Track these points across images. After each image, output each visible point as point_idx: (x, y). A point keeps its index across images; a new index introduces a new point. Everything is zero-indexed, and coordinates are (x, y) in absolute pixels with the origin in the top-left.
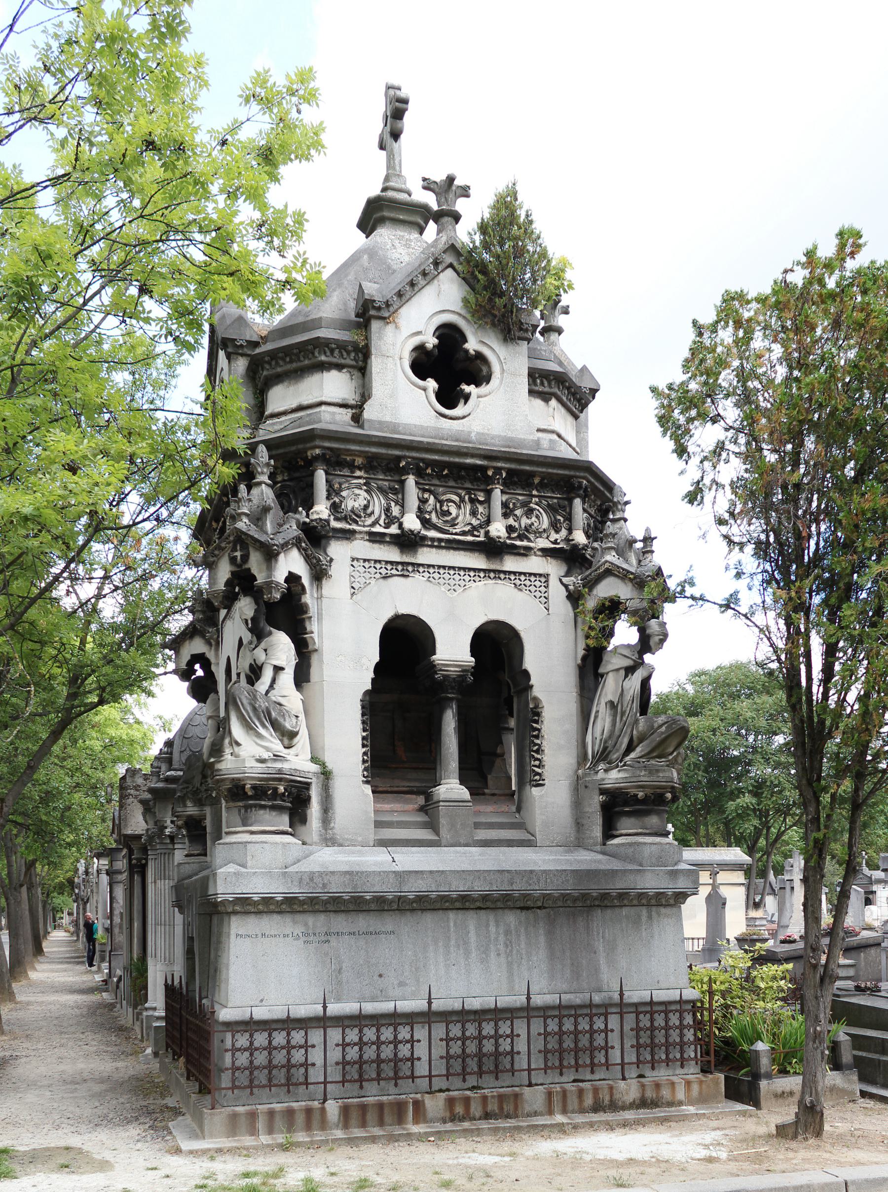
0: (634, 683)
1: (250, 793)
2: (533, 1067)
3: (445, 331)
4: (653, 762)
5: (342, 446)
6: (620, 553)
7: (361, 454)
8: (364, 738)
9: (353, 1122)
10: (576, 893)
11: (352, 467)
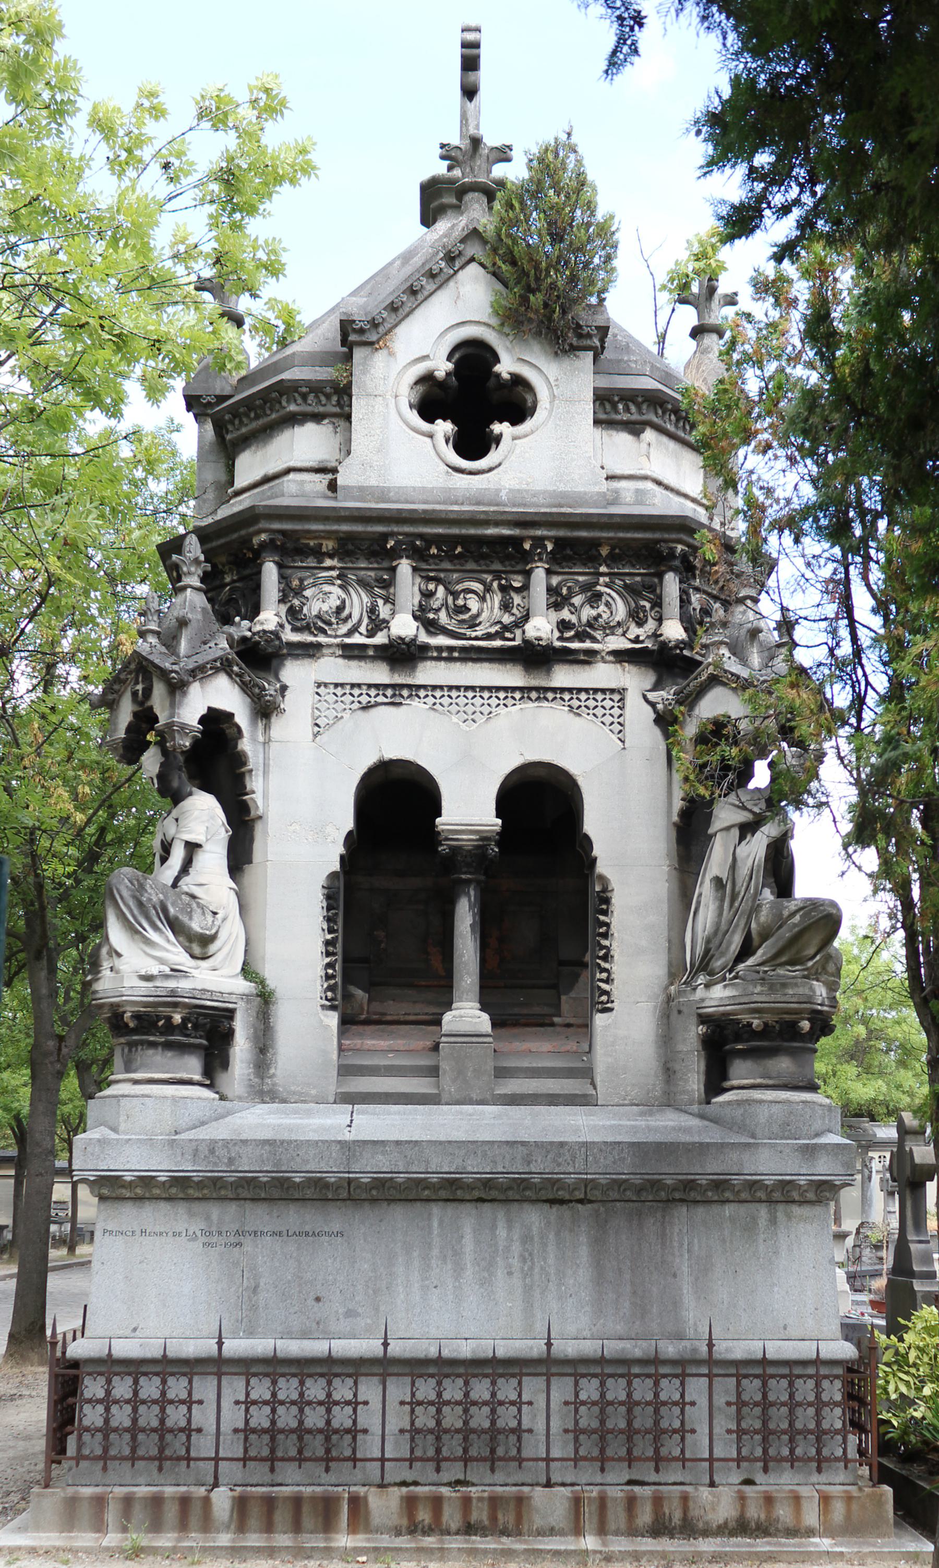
0: (756, 848)
1: (131, 1025)
2: (221, 1455)
3: (469, 350)
4: (781, 971)
5: (298, 526)
6: (737, 650)
7: (328, 535)
8: (327, 943)
9: (253, 1522)
10: (637, 1180)
11: (319, 554)
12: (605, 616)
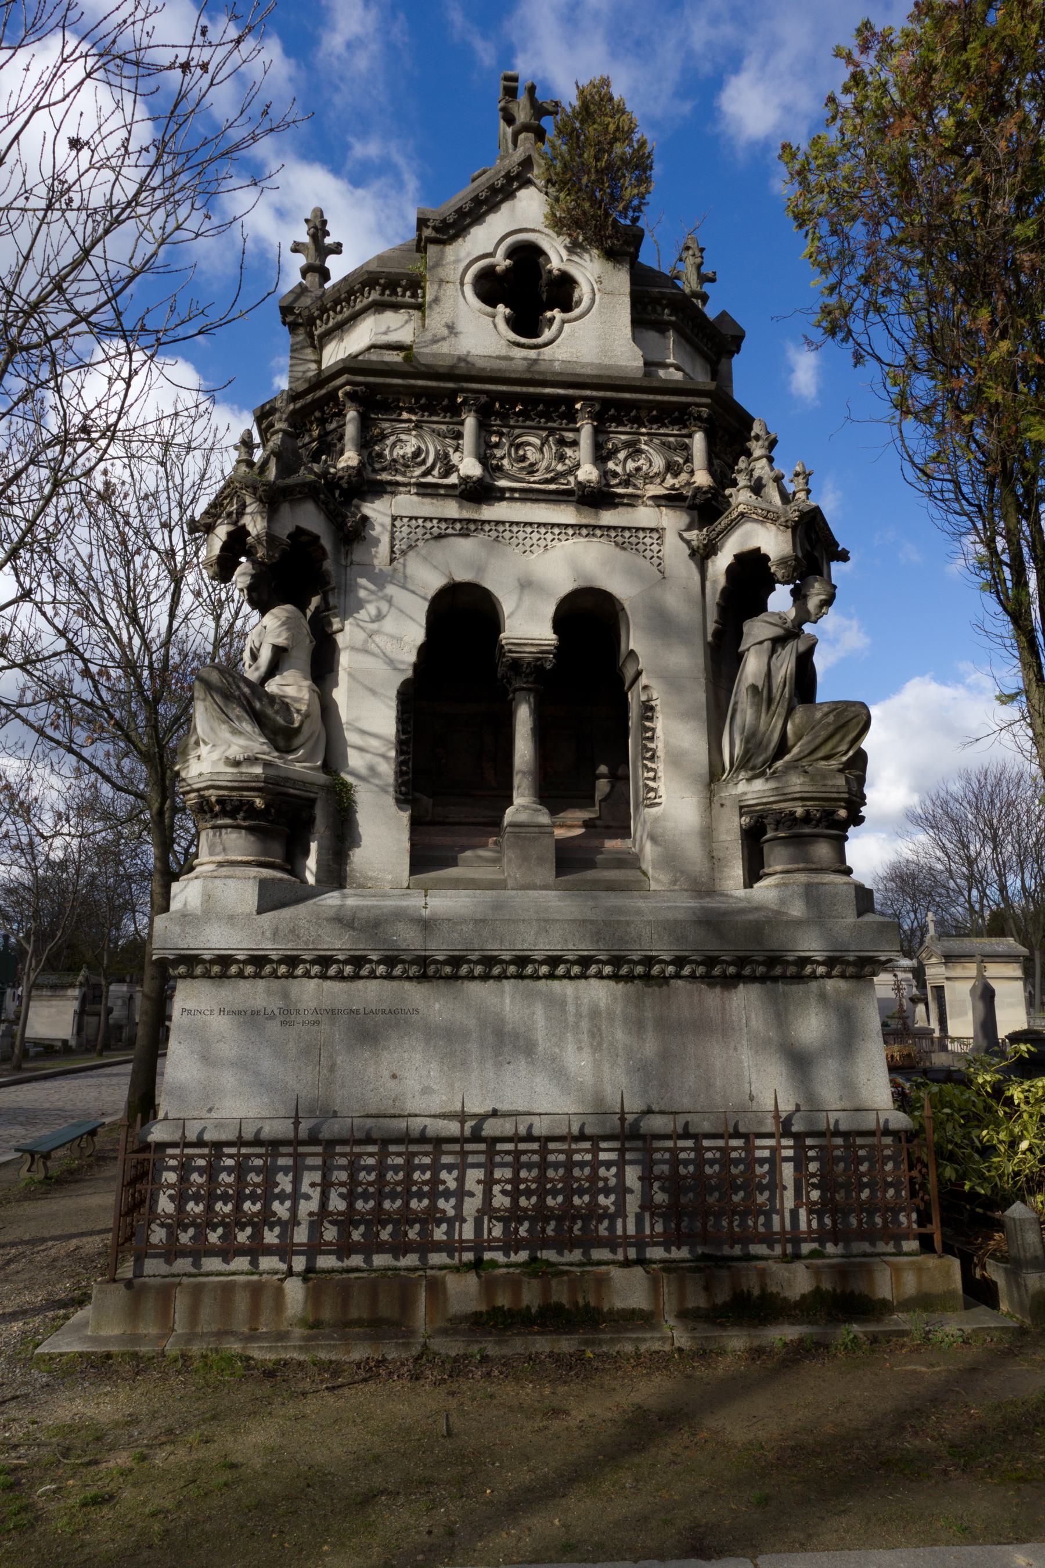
12: (645, 468)
